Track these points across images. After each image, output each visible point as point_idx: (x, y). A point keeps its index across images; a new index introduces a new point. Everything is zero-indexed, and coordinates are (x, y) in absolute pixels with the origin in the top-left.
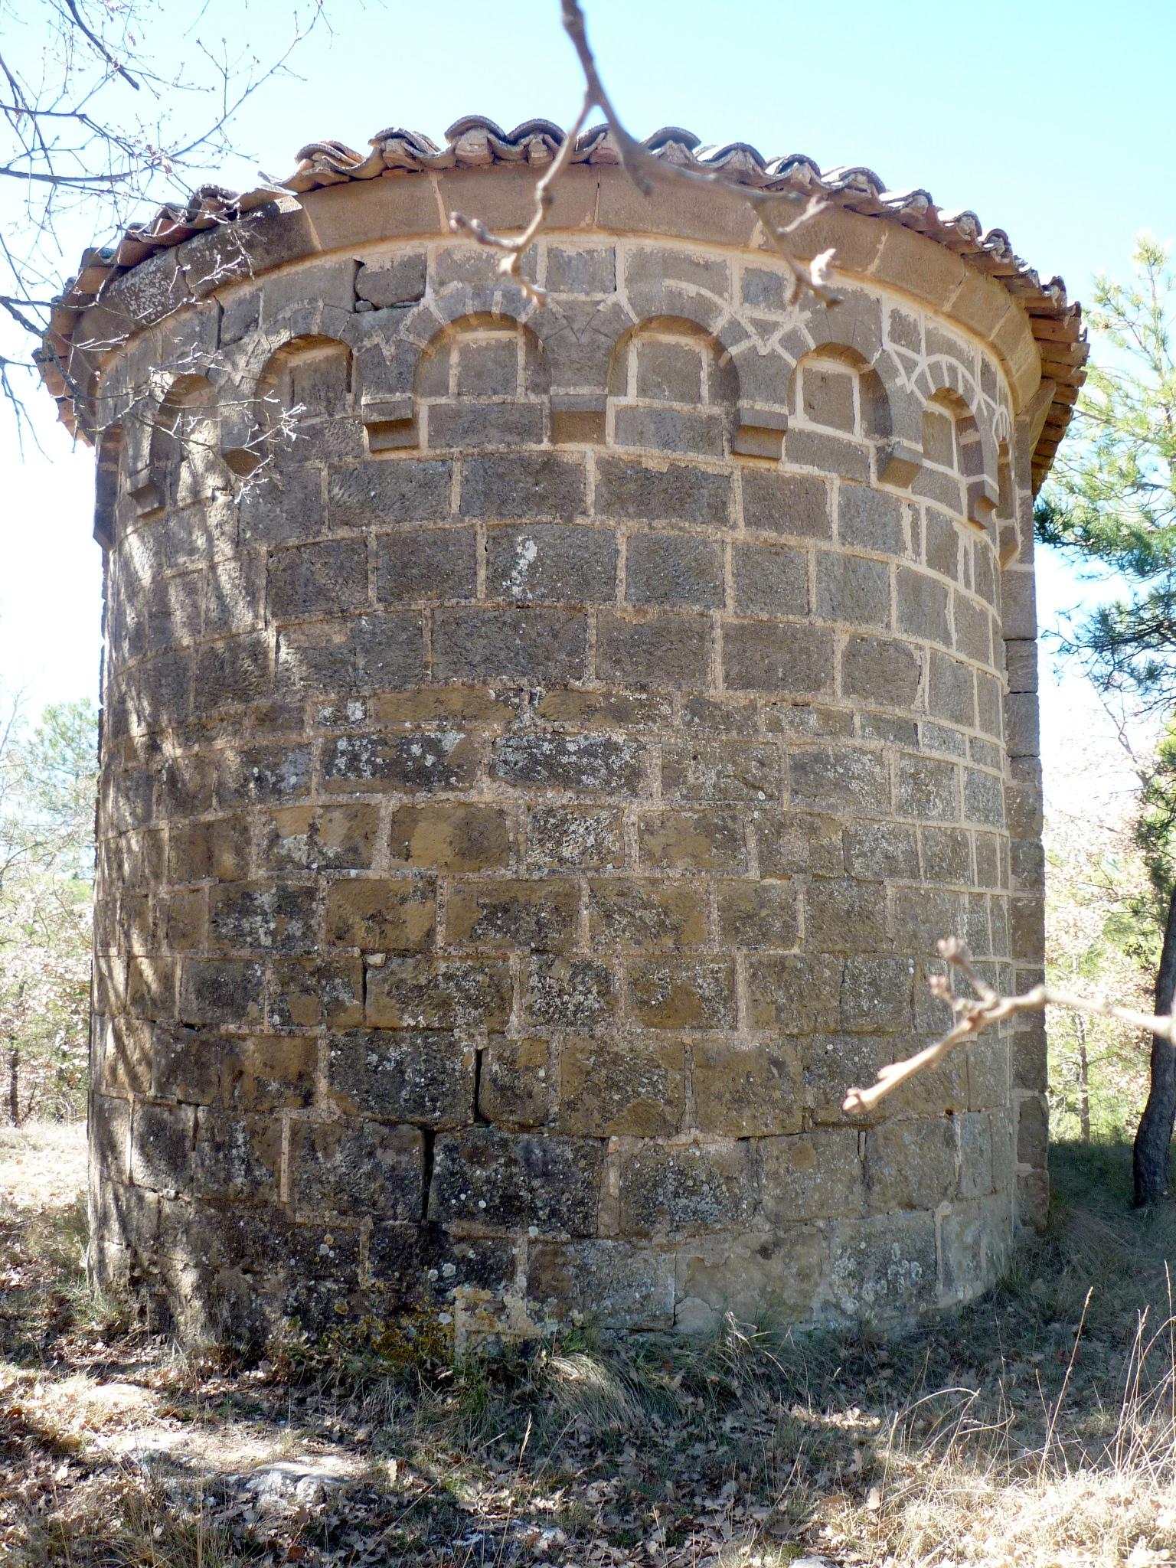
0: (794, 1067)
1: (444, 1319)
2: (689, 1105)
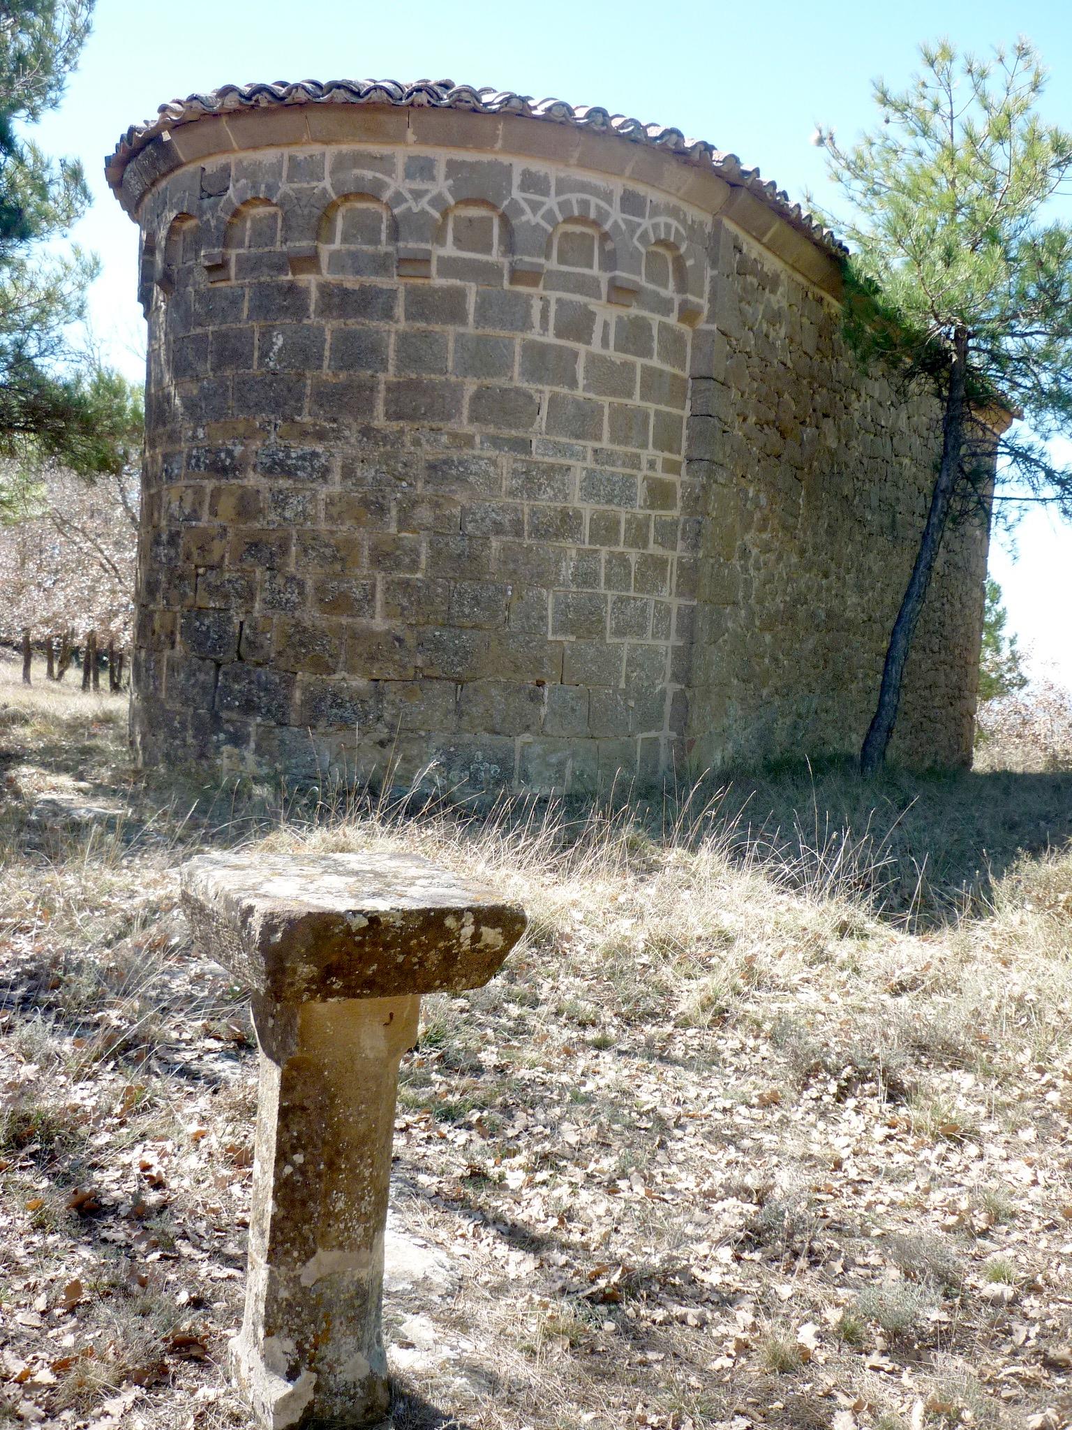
0: (411, 641)
1: (218, 762)
2: (342, 659)
